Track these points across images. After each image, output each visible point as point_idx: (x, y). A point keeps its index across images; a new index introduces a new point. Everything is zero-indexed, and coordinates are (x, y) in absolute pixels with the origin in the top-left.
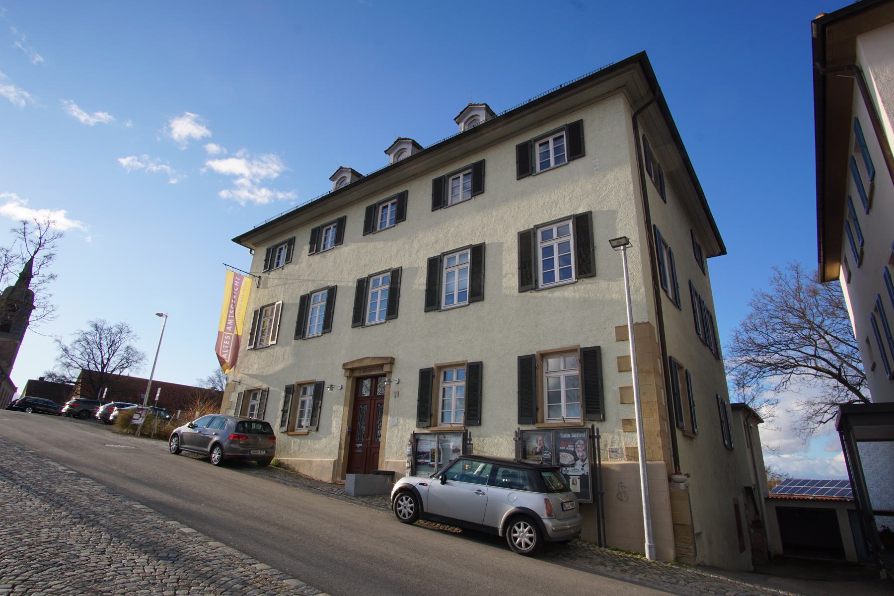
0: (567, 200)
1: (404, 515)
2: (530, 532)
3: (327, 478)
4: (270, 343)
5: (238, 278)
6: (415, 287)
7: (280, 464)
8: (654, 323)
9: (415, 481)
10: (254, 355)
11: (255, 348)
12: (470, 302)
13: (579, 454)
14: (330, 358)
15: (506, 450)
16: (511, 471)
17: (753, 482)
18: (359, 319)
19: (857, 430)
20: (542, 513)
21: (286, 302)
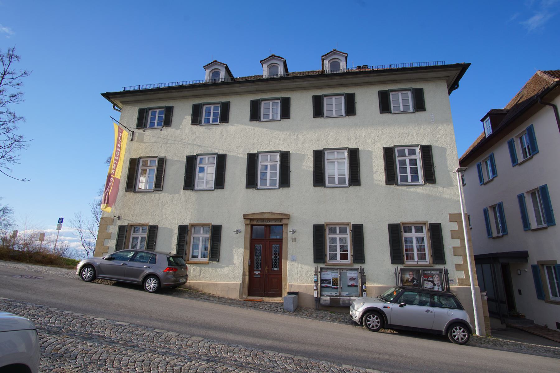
0: (415, 134)
3: (235, 295)
6: (303, 167)
13: (436, 283)
14: (232, 208)
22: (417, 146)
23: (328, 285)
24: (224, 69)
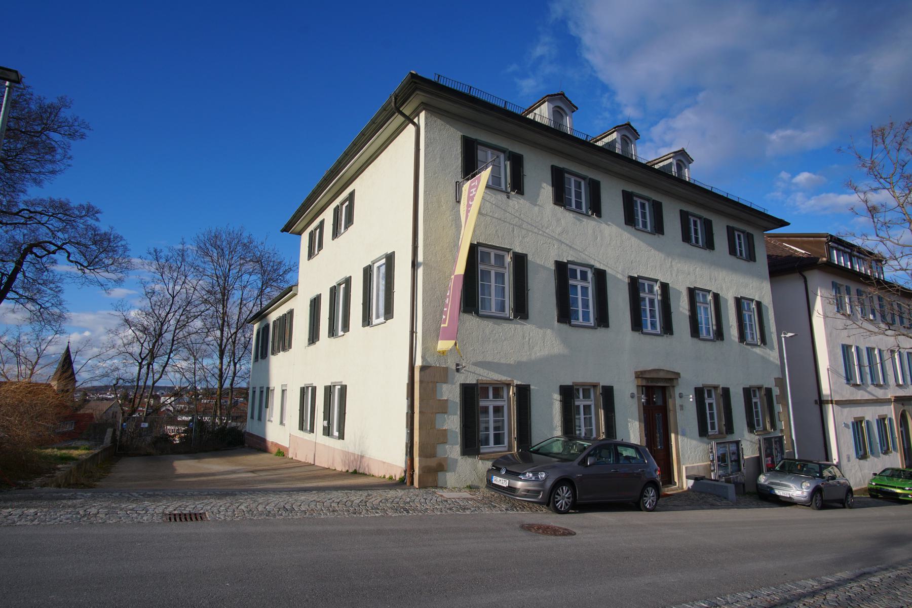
22: (508, 250)
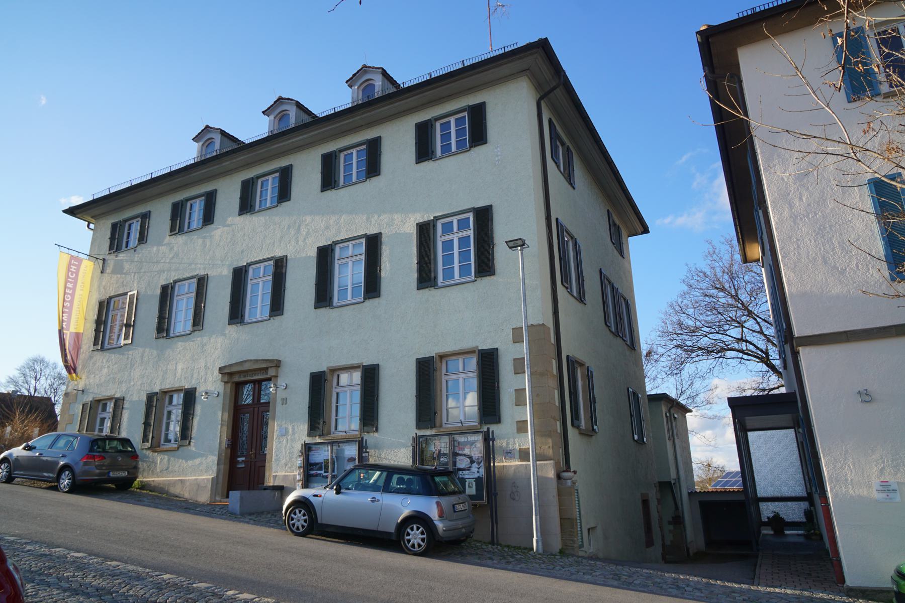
1: (298, 528)
2: (422, 533)
3: (204, 497)
4: (122, 342)
5: (74, 262)
7: (143, 486)
8: (550, 324)
9: (308, 493)
10: (101, 358)
11: (102, 349)
12: (365, 299)
14: (199, 362)
15: (403, 457)
16: (406, 477)
17: (673, 475)
18: (236, 314)
19: (750, 421)
20: (434, 514)
21: (142, 291)
23: (319, 472)
24: (295, 107)
